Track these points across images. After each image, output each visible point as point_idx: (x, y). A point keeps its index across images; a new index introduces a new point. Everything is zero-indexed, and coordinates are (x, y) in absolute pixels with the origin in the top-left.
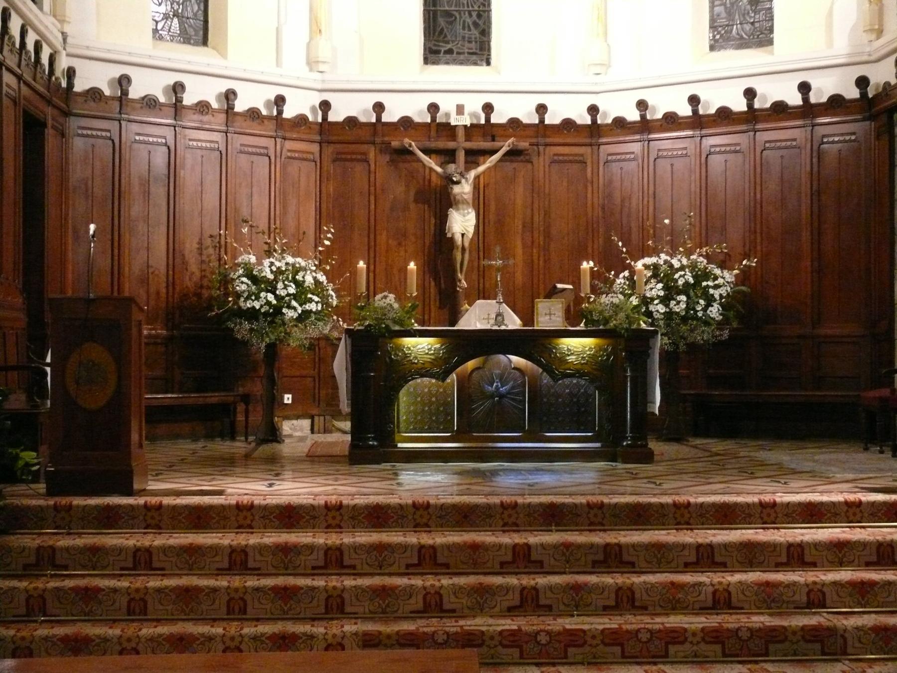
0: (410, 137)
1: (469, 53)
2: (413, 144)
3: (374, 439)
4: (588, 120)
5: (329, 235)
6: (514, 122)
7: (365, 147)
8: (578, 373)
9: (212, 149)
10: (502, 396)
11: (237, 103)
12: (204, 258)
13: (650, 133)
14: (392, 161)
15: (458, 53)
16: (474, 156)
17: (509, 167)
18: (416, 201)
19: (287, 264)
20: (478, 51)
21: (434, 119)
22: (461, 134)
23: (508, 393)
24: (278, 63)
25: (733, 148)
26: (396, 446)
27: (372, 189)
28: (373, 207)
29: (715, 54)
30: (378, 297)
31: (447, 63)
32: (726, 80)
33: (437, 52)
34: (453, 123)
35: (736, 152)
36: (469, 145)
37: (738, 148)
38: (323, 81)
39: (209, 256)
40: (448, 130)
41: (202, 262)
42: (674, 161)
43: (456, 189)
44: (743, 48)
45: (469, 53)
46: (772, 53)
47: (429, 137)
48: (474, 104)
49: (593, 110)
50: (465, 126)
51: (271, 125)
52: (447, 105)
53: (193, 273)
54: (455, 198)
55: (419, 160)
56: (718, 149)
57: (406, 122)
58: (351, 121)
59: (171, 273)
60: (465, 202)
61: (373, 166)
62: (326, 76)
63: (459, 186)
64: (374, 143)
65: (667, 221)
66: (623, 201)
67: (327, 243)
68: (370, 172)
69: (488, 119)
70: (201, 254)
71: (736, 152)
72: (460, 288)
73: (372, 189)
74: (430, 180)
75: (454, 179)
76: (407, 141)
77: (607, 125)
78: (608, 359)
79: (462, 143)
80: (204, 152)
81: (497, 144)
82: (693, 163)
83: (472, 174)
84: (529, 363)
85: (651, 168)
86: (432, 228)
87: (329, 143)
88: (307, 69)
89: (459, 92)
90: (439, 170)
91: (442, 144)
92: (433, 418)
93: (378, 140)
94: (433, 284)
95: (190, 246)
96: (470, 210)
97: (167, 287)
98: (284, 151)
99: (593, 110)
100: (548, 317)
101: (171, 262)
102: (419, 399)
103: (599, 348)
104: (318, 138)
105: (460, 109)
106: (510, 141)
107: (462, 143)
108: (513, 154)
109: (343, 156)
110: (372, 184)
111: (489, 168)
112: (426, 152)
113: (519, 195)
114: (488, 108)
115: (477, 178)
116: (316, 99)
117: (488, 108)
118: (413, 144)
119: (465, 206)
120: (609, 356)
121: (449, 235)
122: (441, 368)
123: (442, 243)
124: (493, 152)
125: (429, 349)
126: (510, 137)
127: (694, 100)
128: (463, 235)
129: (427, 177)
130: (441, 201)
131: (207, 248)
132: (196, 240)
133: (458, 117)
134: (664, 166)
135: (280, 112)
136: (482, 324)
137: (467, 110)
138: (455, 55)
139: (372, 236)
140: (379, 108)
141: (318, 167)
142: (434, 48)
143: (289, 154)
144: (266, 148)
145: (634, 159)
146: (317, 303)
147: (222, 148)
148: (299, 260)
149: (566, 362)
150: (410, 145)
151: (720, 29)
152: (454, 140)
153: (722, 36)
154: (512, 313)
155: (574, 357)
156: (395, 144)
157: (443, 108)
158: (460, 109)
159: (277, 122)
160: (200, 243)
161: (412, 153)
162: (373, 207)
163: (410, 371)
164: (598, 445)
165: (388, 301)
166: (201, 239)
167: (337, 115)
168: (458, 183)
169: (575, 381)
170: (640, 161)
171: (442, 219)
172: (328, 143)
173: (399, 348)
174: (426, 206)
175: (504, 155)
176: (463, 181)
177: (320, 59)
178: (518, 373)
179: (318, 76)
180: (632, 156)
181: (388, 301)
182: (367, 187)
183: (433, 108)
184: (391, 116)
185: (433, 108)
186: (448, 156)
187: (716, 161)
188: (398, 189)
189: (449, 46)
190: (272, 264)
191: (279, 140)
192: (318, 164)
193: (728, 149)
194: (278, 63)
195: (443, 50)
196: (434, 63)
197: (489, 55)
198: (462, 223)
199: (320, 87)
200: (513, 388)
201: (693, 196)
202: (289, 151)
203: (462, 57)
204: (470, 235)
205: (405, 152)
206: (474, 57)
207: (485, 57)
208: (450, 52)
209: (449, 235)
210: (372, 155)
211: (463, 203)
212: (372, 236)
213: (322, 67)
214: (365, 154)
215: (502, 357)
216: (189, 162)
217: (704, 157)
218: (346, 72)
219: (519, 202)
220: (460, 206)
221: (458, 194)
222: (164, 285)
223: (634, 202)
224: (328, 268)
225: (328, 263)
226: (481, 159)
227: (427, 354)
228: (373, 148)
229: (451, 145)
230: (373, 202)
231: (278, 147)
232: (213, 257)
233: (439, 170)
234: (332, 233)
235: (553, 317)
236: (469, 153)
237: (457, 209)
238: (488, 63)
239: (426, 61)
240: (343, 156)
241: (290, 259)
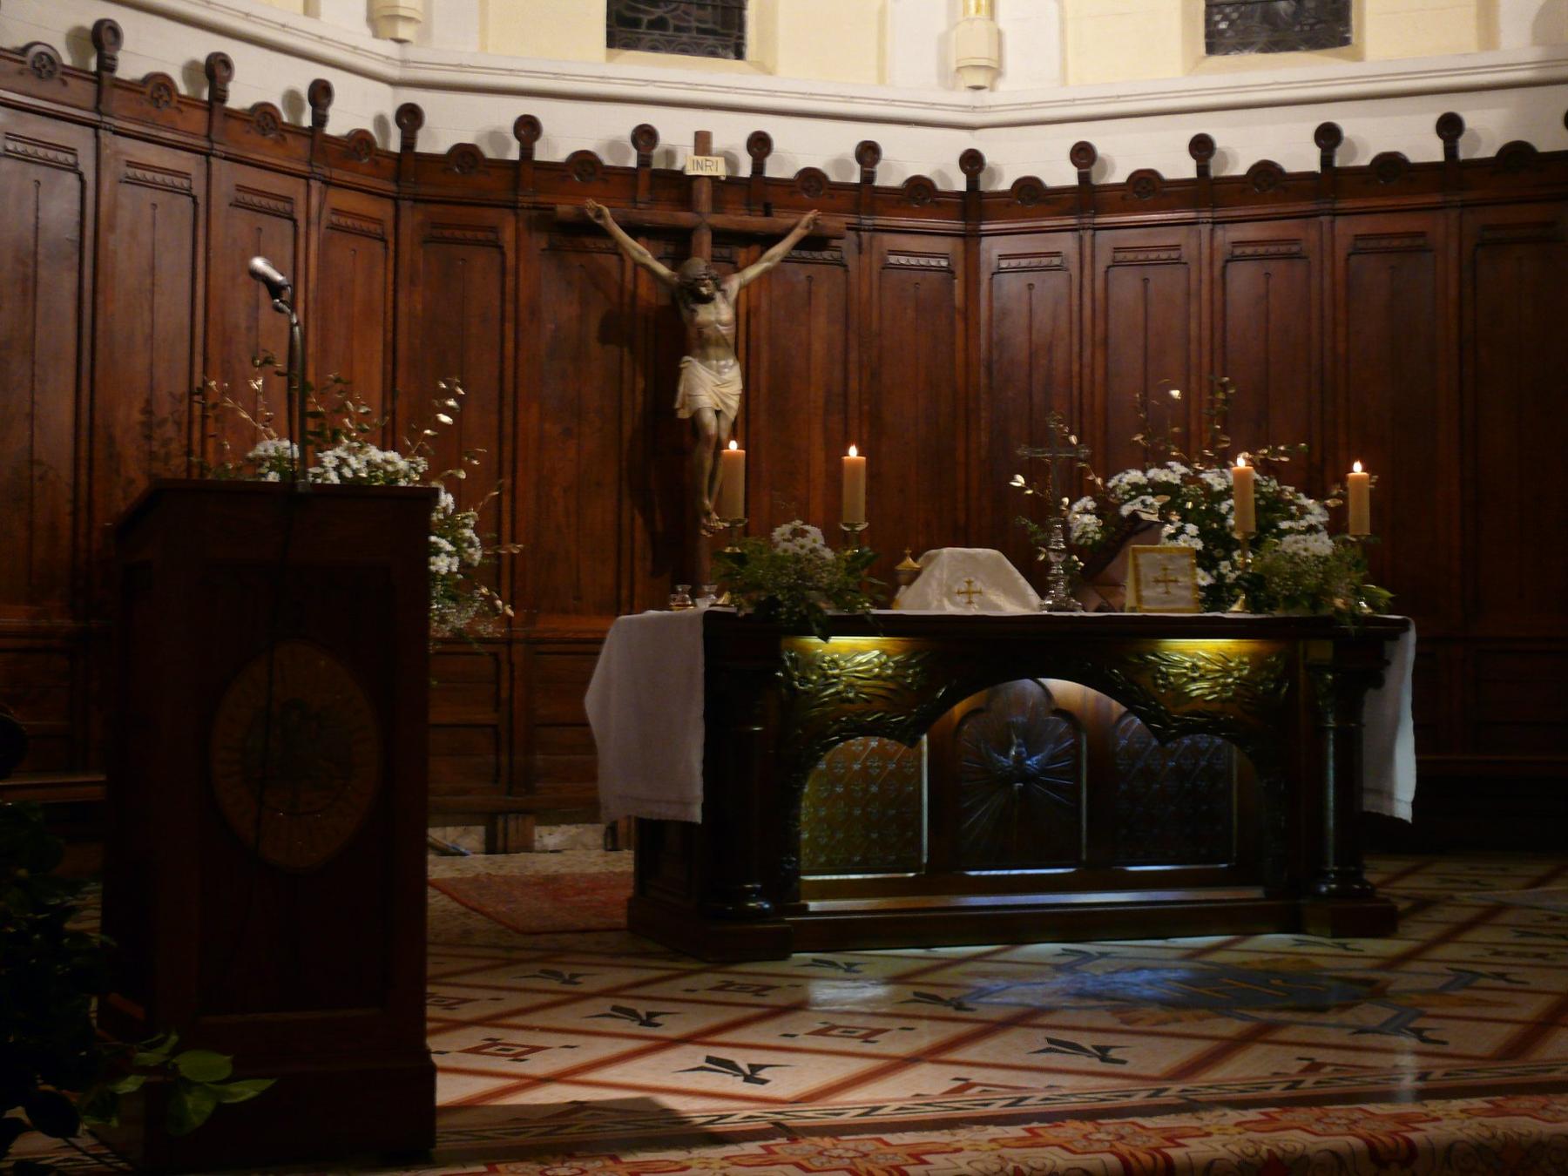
0: (597, 198)
1: (701, 31)
2: (607, 211)
3: (761, 895)
4: (959, 183)
5: (451, 403)
6: (811, 178)
7: (491, 216)
8: (1207, 719)
9: (173, 190)
10: (1028, 778)
11: (232, 88)
12: (156, 447)
13: (1098, 213)
14: (553, 249)
15: (678, 29)
16: (738, 244)
17: (800, 273)
18: (604, 338)
19: (369, 463)
20: (718, 28)
21: (644, 160)
22: (704, 195)
23: (1043, 771)
24: (881, 80)
25: (1283, 249)
26: (804, 910)
27: (510, 307)
28: (510, 346)
29: (1217, 60)
30: (781, 531)
31: (654, 48)
32: (1269, 114)
33: (636, 23)
34: (690, 172)
35: (1290, 256)
36: (719, 220)
37: (1295, 249)
38: (405, 63)
39: (166, 442)
40: (679, 185)
41: (152, 455)
42: (1150, 272)
43: (705, 314)
44: (1281, 50)
45: (701, 31)
46: (1358, 57)
47: (635, 201)
48: (731, 134)
49: (972, 162)
50: (714, 179)
51: (300, 147)
52: (676, 132)
53: (131, 482)
54: (700, 333)
55: (617, 250)
56: (1249, 250)
57: (584, 161)
58: (465, 154)
59: (84, 479)
60: (720, 342)
61: (511, 256)
62: (411, 52)
63: (710, 307)
64: (513, 207)
65: (1176, 393)
66: (1032, 355)
67: (445, 419)
68: (503, 273)
69: (758, 167)
70: (149, 438)
71: (1290, 256)
72: (709, 529)
73: (510, 307)
74: (634, 295)
75: (704, 290)
76: (591, 203)
77: (1003, 194)
78: (1278, 689)
79: (706, 216)
80: (159, 196)
81: (781, 220)
82: (1194, 276)
83: (734, 284)
84: (1092, 692)
85: (1099, 284)
86: (640, 399)
87: (416, 200)
88: (368, 32)
89: (693, 108)
90: (663, 269)
91: (663, 215)
92: (877, 834)
93: (525, 200)
94: (639, 521)
95: (128, 415)
96: (731, 362)
97: (75, 513)
98: (325, 214)
99: (972, 162)
100: (1161, 589)
101: (83, 454)
102: (874, 789)
103: (1258, 662)
104: (391, 187)
105: (702, 142)
106: (811, 215)
107: (706, 216)
108: (814, 242)
109: (447, 233)
110: (509, 296)
111: (767, 273)
112: (634, 231)
113: (821, 329)
114: (760, 144)
115: (746, 287)
116: (387, 102)
117: (760, 144)
118: (607, 211)
119: (721, 352)
120: (1279, 682)
121: (684, 414)
122: (900, 708)
123: (670, 436)
124: (773, 239)
125: (883, 665)
126: (810, 209)
127: (1202, 147)
128: (718, 413)
129: (630, 286)
130: (668, 337)
131: (163, 422)
132: (139, 404)
133: (700, 158)
134: (1126, 285)
135: (320, 120)
136: (955, 604)
137: (717, 144)
138: (670, 32)
139: (508, 414)
140: (528, 128)
141: (391, 254)
142: (629, 14)
143: (334, 218)
144: (288, 200)
145: (1059, 268)
146: (449, 554)
147: (199, 190)
148: (392, 455)
149: (1187, 697)
150: (600, 215)
151: (1228, 10)
152: (690, 210)
153: (1232, 23)
154: (1023, 581)
155: (1205, 685)
156: (564, 209)
157: (666, 138)
158: (702, 142)
159: (296, 143)
160: (148, 410)
161: (604, 233)
162: (510, 346)
163: (837, 720)
164: (1256, 893)
165: (807, 542)
166: (148, 402)
167: (436, 139)
168: (708, 299)
169: (874, 744)
170: (1075, 272)
171: (666, 380)
172: (415, 201)
173: (809, 662)
174: (626, 350)
175: (799, 246)
176: (718, 295)
177: (402, 12)
178: (1063, 727)
179: (387, 48)
180: (1056, 261)
181: (807, 542)
182: (498, 303)
183: (645, 136)
184: (555, 147)
185: (645, 136)
186: (677, 243)
187: (1243, 278)
188: (558, 306)
189: (658, 12)
190: (343, 462)
191: (315, 185)
192: (391, 247)
193: (1272, 249)
194: (881, 80)
195: (646, 19)
196: (628, 45)
197: (742, 38)
198: (714, 387)
199: (395, 72)
200: (1053, 759)
201: (1194, 346)
202: (336, 211)
203: (685, 37)
204: (732, 415)
205: (587, 229)
206: (710, 40)
207: (733, 41)
208: (659, 24)
209: (684, 414)
210: (508, 236)
211: (718, 345)
212: (508, 414)
213: (404, 31)
214: (493, 229)
215: (1028, 684)
216: (124, 217)
217: (1218, 264)
218: (451, 46)
219: (818, 347)
220: (712, 351)
221: (709, 324)
222: (68, 508)
223: (1060, 354)
224: (463, 475)
225: (460, 466)
226: (742, 254)
227: (877, 677)
228: (512, 218)
229: (684, 218)
230: (510, 334)
231: (314, 201)
232: (174, 446)
233: (663, 269)
234: (458, 398)
235: (1173, 589)
236: (723, 237)
237: (704, 358)
238: (739, 54)
239: (613, 41)
240: (447, 233)
241: (376, 454)
